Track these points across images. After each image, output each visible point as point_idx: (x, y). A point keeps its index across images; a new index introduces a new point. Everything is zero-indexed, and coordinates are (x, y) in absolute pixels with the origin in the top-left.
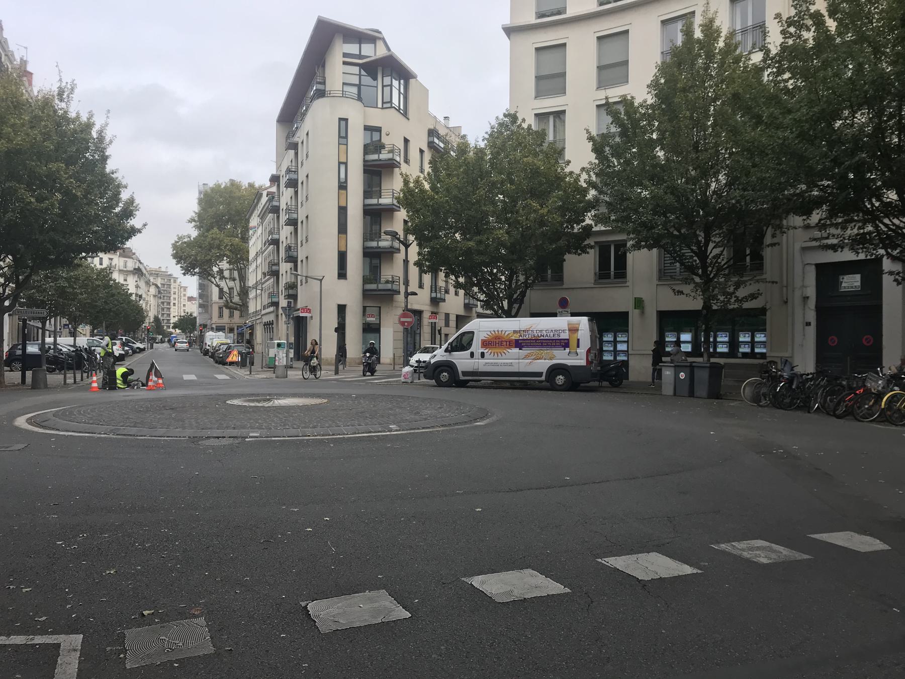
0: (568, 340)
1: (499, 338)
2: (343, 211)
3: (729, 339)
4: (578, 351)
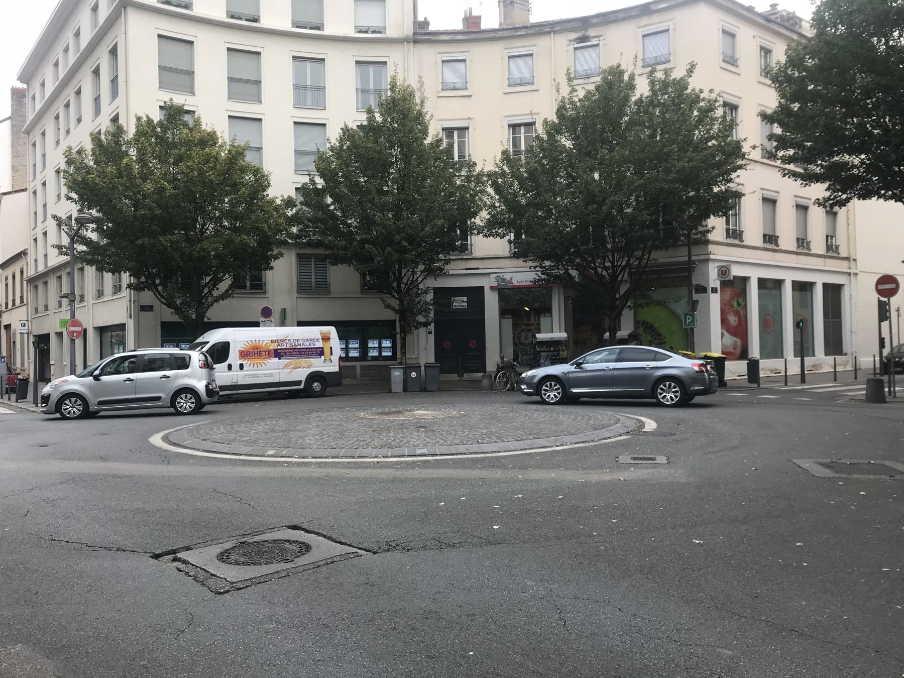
0: (322, 348)
1: (257, 349)
2: (478, 269)
3: (360, 345)
4: (332, 357)
